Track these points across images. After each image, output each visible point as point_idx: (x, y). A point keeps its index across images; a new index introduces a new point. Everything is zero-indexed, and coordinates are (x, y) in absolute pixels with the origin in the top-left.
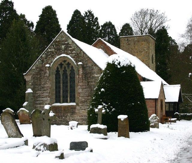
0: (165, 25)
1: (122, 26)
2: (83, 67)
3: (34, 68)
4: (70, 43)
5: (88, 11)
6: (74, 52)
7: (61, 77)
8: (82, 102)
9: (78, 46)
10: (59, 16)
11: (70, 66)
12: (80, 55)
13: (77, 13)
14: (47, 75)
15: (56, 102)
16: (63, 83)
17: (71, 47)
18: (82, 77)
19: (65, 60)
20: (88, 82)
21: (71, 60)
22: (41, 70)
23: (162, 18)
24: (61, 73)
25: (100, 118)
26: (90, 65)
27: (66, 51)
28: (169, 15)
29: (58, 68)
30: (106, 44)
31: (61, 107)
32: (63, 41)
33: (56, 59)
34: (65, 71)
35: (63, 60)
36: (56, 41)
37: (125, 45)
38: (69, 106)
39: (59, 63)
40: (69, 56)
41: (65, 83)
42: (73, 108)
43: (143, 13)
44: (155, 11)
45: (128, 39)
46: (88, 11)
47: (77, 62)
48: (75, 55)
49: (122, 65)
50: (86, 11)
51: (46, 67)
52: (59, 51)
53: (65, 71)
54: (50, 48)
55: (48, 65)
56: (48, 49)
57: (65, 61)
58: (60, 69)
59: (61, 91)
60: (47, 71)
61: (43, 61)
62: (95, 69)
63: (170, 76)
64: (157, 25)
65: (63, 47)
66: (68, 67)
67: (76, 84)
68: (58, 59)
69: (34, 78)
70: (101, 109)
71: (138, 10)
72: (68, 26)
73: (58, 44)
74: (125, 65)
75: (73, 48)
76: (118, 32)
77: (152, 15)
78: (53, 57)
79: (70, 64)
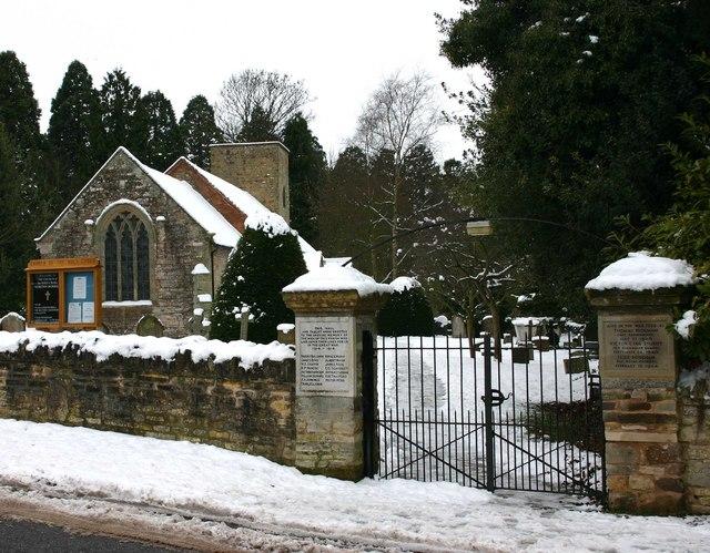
0: (305, 110)
1: (188, 102)
2: (167, 226)
3: (59, 226)
4: (138, 174)
5: (115, 72)
6: (147, 194)
7: (119, 248)
8: (165, 299)
9: (155, 183)
10: (33, 79)
11: (138, 223)
12: (160, 201)
13: (77, 72)
14: (89, 242)
15: (108, 299)
16: (123, 259)
17: (140, 184)
18: (165, 247)
19: (126, 210)
20: (179, 258)
21: (141, 212)
22: (74, 231)
23: (297, 93)
24: (118, 237)
25: (244, 329)
26: (181, 222)
27: (129, 191)
28: (311, 87)
29: (110, 227)
30: (196, 171)
31: (119, 309)
32: (122, 171)
33: (107, 208)
34: (126, 235)
35: (123, 210)
36: (108, 172)
37: (222, 164)
38: (137, 307)
39: (114, 217)
40: (135, 203)
41: (127, 260)
42: (144, 309)
43: (252, 81)
44: (281, 77)
45: (228, 152)
46: (115, 72)
47: (152, 214)
48: (149, 201)
49: (275, 232)
50: (111, 72)
51: (85, 226)
52: (113, 192)
53: (126, 235)
54: (93, 186)
55: (89, 222)
56: (88, 187)
57: (126, 213)
58: (115, 229)
59: (119, 275)
60: (88, 233)
61: (78, 213)
62: (194, 232)
63: (317, 234)
64: (284, 109)
65: (123, 183)
66: (134, 225)
67: (151, 262)
68: (111, 208)
69: (58, 249)
70: (242, 312)
71: (238, 72)
72: (54, 102)
73: (111, 176)
74: (281, 233)
75: (144, 185)
76: (179, 115)
77: (272, 86)
78: (101, 204)
79: (138, 219)
